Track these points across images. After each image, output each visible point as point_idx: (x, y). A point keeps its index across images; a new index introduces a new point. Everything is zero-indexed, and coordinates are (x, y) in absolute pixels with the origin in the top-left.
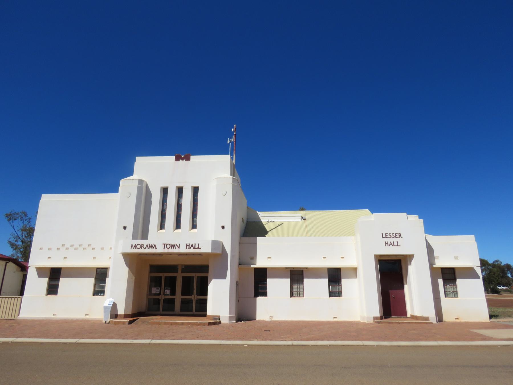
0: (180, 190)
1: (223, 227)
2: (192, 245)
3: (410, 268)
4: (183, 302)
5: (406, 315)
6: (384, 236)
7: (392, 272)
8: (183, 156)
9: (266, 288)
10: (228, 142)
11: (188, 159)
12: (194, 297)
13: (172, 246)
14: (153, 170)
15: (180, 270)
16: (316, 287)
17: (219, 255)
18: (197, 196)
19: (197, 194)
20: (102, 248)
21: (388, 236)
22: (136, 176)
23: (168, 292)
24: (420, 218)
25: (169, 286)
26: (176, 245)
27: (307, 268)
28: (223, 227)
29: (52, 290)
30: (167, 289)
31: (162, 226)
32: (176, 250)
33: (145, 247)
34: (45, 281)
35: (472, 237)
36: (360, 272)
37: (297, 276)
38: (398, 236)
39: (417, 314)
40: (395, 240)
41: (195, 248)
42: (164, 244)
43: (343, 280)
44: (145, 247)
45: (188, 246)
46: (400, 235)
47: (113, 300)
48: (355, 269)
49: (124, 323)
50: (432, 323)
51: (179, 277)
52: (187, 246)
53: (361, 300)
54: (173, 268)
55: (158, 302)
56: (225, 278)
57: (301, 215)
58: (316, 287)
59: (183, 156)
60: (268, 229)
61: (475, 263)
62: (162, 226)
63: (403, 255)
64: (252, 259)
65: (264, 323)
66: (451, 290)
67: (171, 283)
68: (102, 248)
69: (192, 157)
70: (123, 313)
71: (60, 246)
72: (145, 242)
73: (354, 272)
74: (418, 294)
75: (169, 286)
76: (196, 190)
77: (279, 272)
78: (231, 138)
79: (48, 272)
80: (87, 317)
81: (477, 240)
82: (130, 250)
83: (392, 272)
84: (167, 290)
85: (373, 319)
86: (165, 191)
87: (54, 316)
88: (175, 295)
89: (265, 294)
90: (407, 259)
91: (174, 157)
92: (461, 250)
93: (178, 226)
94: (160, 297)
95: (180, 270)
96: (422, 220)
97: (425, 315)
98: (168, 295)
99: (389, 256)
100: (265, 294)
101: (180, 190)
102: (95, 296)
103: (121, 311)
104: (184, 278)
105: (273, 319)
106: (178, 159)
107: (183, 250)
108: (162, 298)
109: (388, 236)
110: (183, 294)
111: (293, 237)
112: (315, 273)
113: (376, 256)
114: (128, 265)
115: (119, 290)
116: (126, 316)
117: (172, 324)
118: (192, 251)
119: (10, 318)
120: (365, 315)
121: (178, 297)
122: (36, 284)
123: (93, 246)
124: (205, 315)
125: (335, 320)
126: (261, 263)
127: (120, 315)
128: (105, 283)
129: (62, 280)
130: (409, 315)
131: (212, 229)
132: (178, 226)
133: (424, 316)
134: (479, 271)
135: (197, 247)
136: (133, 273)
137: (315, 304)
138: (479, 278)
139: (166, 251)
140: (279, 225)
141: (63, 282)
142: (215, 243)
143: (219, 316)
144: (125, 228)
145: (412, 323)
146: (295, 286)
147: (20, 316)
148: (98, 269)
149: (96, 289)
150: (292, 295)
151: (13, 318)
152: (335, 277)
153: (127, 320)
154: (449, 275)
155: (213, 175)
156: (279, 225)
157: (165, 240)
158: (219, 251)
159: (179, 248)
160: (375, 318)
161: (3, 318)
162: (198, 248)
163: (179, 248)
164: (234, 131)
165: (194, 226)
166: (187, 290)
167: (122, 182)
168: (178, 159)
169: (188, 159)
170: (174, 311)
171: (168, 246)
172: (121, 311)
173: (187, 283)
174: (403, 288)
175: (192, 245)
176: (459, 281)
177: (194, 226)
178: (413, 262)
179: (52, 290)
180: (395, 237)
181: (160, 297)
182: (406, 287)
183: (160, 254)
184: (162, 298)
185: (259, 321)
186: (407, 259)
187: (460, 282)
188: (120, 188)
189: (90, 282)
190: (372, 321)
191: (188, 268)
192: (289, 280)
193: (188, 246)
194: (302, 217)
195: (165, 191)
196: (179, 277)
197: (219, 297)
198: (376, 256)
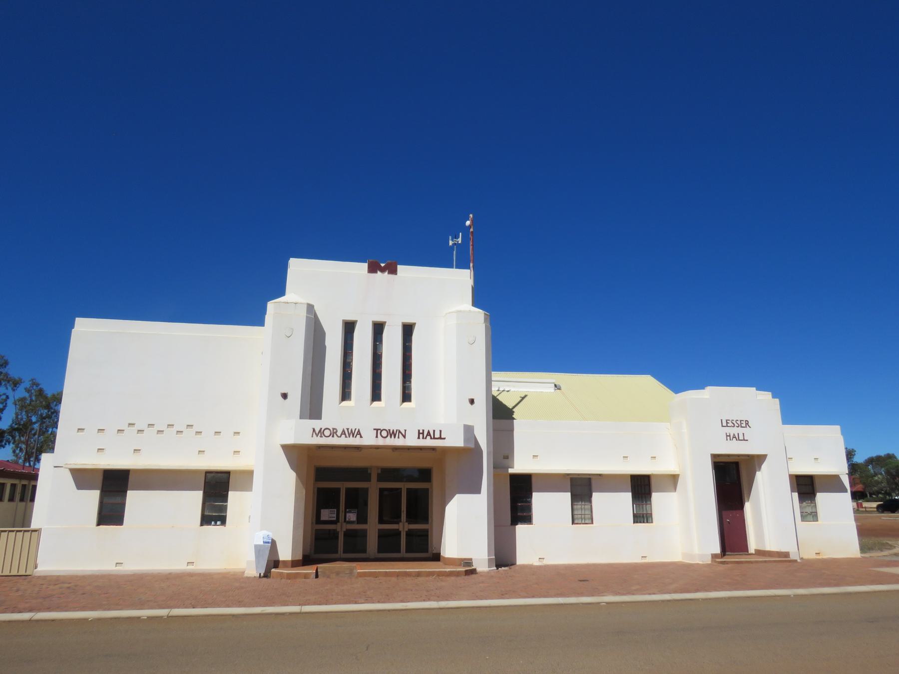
0: (378, 329)
1: (472, 402)
2: (429, 432)
3: (759, 475)
4: (382, 535)
5: (747, 551)
6: (725, 424)
7: (732, 480)
8: (383, 265)
9: (529, 508)
10: (451, 243)
11: (393, 271)
12: (404, 527)
13: (392, 434)
14: (322, 286)
15: (374, 477)
16: (613, 506)
17: (471, 452)
18: (381, 341)
19: (414, 341)
20: (217, 433)
21: (730, 424)
22: (291, 295)
23: (352, 517)
24: (773, 397)
25: (368, 507)
26: (400, 432)
27: (600, 475)
28: (472, 402)
29: (111, 514)
30: (350, 512)
31: (345, 395)
32: (398, 442)
33: (339, 433)
34: (92, 498)
35: (837, 428)
36: (258, 480)
37: (581, 488)
38: (744, 425)
39: (771, 545)
40: (740, 431)
41: (434, 438)
42: (377, 430)
43: (231, 494)
44: (339, 433)
45: (420, 434)
46: (747, 423)
47: (265, 533)
48: (249, 474)
49: (306, 576)
50: (796, 561)
51: (373, 489)
52: (419, 433)
53: (685, 529)
54: (362, 474)
55: (334, 535)
56: (477, 491)
57: (553, 381)
58: (613, 506)
59: (383, 265)
60: (510, 405)
61: (839, 467)
62: (345, 395)
63: (748, 456)
64: (506, 457)
65: (530, 569)
66: (809, 510)
67: (357, 500)
68: (217, 433)
69: (400, 268)
70: (290, 559)
71: (124, 427)
72: (317, 424)
73: (672, 480)
74: (770, 518)
75: (368, 507)
76: (408, 330)
77: (553, 482)
78: (457, 237)
79: (100, 478)
80: (119, 568)
81: (843, 433)
82: (290, 441)
83: (732, 480)
84: (351, 515)
85: (710, 557)
86: (349, 328)
87: (119, 568)
88: (427, 523)
89: (528, 520)
90: (755, 461)
91: (366, 265)
92: (823, 449)
93: (376, 395)
94: (338, 527)
95: (374, 477)
96: (777, 401)
97: (784, 549)
98: (352, 522)
99: (729, 456)
100: (528, 520)
101: (378, 329)
102: (205, 527)
103: (286, 553)
104: (382, 491)
105: (546, 562)
106: (373, 269)
107: (412, 441)
108: (341, 528)
109: (730, 424)
110: (381, 521)
111: (577, 419)
112: (609, 483)
113: (714, 456)
114: (294, 466)
115: (269, 515)
116: (294, 564)
117: (398, 575)
118: (428, 442)
119: (14, 572)
120: (696, 551)
121: (373, 528)
122: (59, 503)
123: (195, 429)
124: (437, 557)
125: (644, 561)
126: (521, 465)
127: (284, 562)
128: (226, 501)
129: (656, 497)
130: (752, 550)
131: (442, 404)
132: (376, 395)
133: (783, 550)
134: (846, 480)
135: (437, 435)
136: (301, 485)
137: (611, 536)
138: (846, 491)
139: (380, 442)
140: (523, 398)
141: (135, 499)
142: (469, 430)
143: (471, 559)
144: (285, 396)
145: (757, 562)
146: (578, 506)
147: (39, 569)
148: (207, 473)
149: (207, 513)
150: (573, 523)
151: (22, 572)
152: (641, 487)
153: (310, 570)
154: (806, 487)
155: (440, 303)
156: (523, 398)
157: (361, 421)
158: (472, 446)
159: (404, 437)
160: (714, 556)
161: (6, 573)
162: (440, 438)
163: (404, 437)
164: (470, 227)
165: (406, 397)
166: (389, 512)
167: (271, 306)
168: (373, 269)
169: (393, 271)
170: (365, 551)
171: (384, 434)
172: (286, 553)
173: (389, 499)
174: (741, 507)
175: (429, 432)
176: (596, 496)
177: (406, 397)
178: (764, 466)
179: (111, 514)
180: (740, 426)
181: (338, 527)
182: (748, 506)
183: (377, 448)
184: (341, 528)
185: (524, 567)
186: (755, 461)
187: (820, 497)
188: (266, 317)
189: (193, 500)
190: (708, 560)
191: (388, 474)
192: (569, 494)
193: (420, 434)
194: (556, 386)
195: (349, 328)
196: (373, 489)
197: (464, 525)
198: (714, 456)
